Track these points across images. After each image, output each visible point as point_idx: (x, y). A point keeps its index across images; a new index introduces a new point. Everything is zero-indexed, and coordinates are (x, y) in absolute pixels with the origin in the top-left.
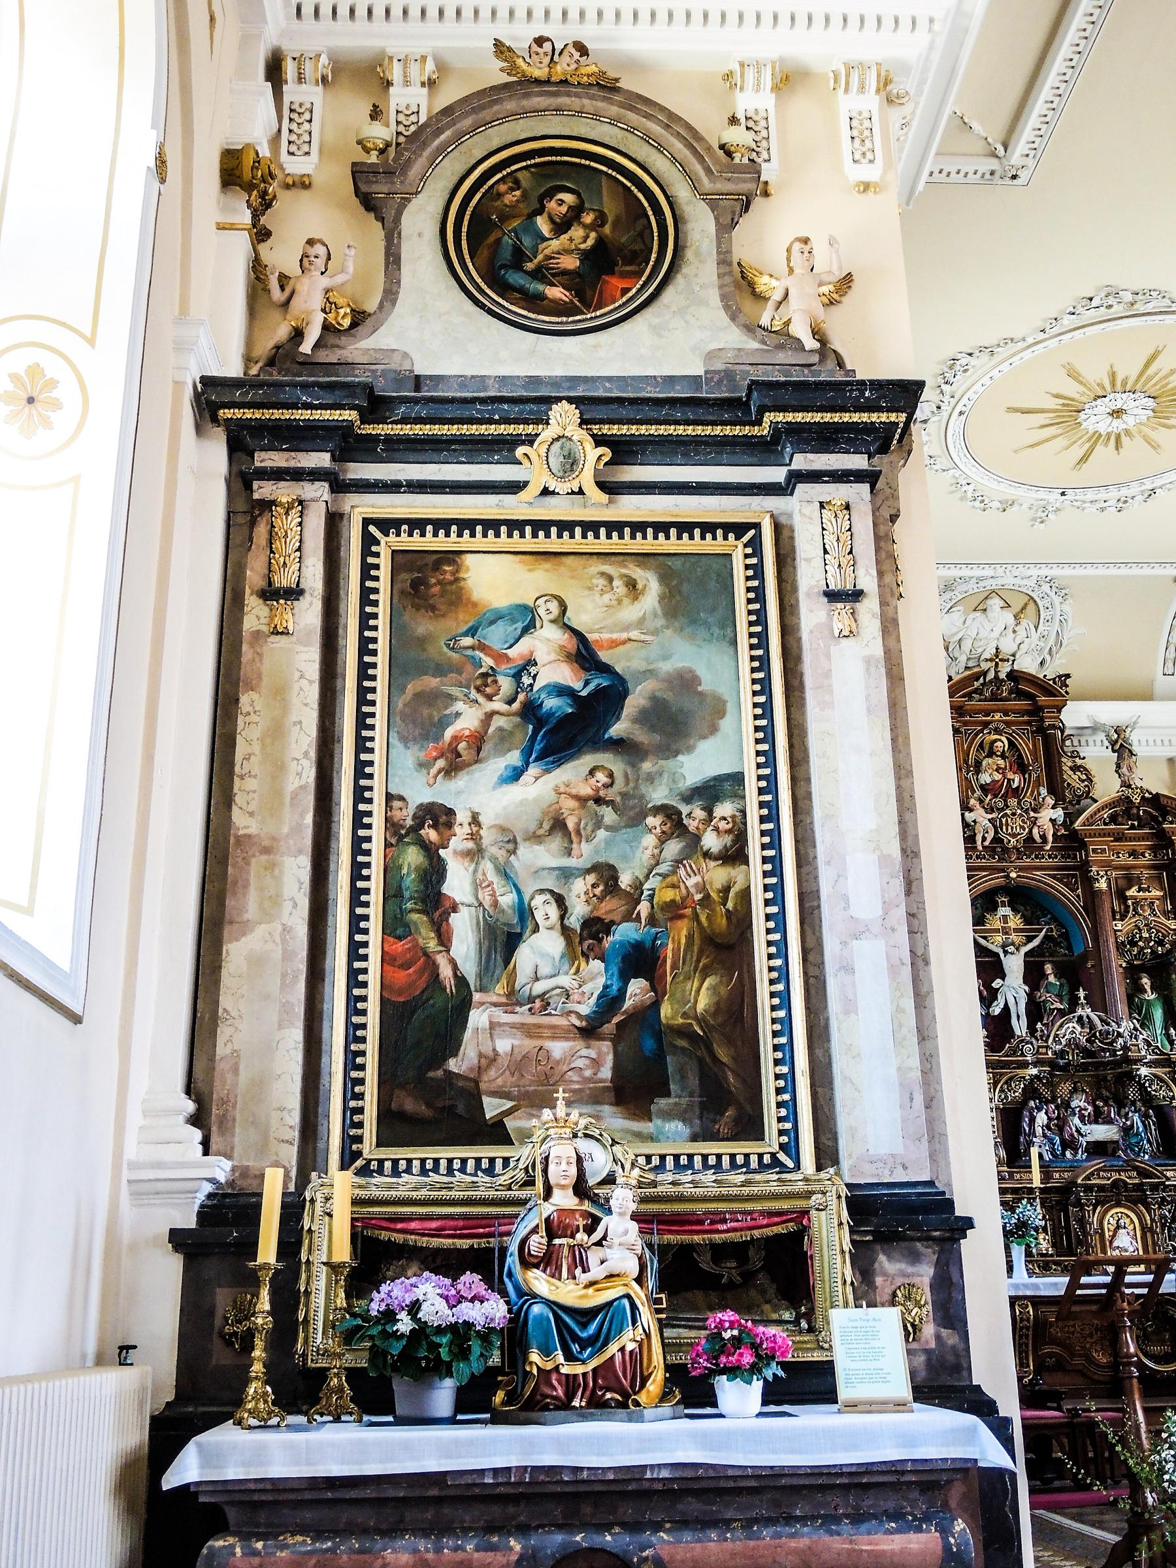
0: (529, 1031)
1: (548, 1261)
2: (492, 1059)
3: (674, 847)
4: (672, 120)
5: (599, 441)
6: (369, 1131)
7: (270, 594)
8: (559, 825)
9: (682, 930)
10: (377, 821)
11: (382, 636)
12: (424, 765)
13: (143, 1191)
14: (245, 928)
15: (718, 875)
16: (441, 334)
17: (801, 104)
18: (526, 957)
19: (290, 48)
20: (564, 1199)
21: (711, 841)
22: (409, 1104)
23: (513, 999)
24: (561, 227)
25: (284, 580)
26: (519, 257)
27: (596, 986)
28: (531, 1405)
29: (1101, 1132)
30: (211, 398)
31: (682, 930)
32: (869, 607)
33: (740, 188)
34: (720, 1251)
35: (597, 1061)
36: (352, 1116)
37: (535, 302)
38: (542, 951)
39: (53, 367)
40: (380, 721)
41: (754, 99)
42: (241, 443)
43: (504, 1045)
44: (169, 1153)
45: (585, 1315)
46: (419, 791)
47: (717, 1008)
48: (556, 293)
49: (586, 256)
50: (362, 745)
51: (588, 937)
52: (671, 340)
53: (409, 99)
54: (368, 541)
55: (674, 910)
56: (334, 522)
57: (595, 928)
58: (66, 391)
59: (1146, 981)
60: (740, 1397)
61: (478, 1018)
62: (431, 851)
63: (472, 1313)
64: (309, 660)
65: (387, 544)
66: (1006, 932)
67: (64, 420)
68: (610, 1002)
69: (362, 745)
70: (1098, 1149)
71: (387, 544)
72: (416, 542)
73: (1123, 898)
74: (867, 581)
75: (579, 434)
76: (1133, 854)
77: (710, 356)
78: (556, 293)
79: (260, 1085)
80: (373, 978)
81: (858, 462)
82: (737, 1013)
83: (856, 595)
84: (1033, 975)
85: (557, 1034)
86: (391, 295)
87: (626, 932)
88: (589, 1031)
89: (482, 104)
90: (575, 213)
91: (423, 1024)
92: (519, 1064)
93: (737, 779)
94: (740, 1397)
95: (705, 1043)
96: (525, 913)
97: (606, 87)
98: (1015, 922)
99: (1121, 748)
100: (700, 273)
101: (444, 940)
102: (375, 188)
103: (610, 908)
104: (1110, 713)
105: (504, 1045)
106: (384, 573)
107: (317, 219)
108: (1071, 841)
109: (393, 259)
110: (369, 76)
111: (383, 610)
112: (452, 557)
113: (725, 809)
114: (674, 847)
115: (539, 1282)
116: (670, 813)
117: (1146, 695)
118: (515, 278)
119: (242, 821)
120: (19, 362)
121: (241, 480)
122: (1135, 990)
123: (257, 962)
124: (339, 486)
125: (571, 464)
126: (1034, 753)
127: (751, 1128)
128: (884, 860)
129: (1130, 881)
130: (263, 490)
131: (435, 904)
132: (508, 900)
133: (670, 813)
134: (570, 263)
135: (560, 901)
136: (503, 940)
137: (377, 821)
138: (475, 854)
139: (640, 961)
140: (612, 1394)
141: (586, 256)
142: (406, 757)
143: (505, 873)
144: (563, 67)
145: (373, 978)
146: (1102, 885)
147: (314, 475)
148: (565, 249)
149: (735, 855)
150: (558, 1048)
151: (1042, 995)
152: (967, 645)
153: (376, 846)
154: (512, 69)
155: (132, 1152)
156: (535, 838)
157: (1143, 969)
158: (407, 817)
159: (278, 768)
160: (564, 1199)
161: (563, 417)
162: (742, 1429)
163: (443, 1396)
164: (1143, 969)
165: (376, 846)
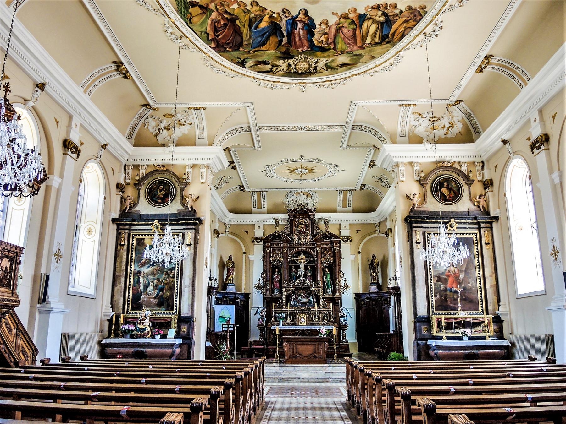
0: (148, 298)
1: (140, 324)
2: (144, 301)
3: (167, 276)
4: (176, 175)
5: (161, 224)
6: (130, 309)
7: (121, 245)
8: (153, 273)
9: (167, 286)
10: (132, 273)
11: (134, 249)
12: (138, 266)
13: (105, 315)
14: (117, 286)
15: (172, 279)
16: (145, 207)
17: (196, 169)
18: (149, 289)
19: (127, 164)
20: (143, 318)
21: (171, 275)
22: (134, 306)
23: (147, 294)
24: (161, 191)
25: (123, 243)
26: (155, 195)
27: (156, 293)
28: (137, 337)
29: (305, 300)
30: (114, 220)
31: (167, 286)
32: (192, 246)
33: (184, 185)
34: (166, 323)
35: (155, 301)
36: (128, 307)
37: (157, 203)
38: (150, 288)
39: (92, 227)
40: (133, 261)
41: (189, 170)
42: (118, 225)
43: (145, 299)
44: (108, 311)
45: (142, 329)
46: (138, 269)
47: (170, 295)
48: (159, 201)
49: (163, 195)
50: (131, 264)
51: (155, 287)
52: (174, 208)
53: (143, 171)
54: (133, 237)
55: (166, 284)
56: (129, 234)
57: (157, 286)
58: (93, 230)
59: (327, 270)
60: (158, 337)
61: (143, 296)
62: (138, 276)
63: (131, 328)
64: (125, 253)
65: (473, 236)
66: (302, 259)
67: (93, 234)
68: (158, 295)
69: (131, 264)
70: (304, 303)
71: (473, 236)
72: (139, 237)
73: (324, 254)
74: (192, 243)
75: (158, 224)
76: (327, 244)
77: (178, 210)
78: (159, 201)
79: (118, 304)
80: (131, 292)
81: (193, 227)
82: (172, 296)
83: (190, 245)
84: (306, 268)
85: (151, 298)
86: (138, 202)
87: (160, 286)
88: (155, 298)
89: (151, 173)
90: (163, 188)
91: (137, 297)
92: (147, 301)
93: (175, 267)
94: (158, 337)
95: (168, 299)
96: (149, 284)
97: (168, 171)
98: (304, 257)
99: (326, 223)
100: (178, 198)
101: (140, 287)
102: (137, 186)
103: (158, 283)
104: (325, 215)
105: (145, 299)
106: (135, 241)
107: (130, 192)
108: (313, 243)
109: (139, 197)
110: (137, 167)
111: (134, 246)
112: (143, 239)
113: (173, 271)
114: (167, 276)
115: (139, 326)
116: (167, 272)
117: (335, 211)
118: (154, 199)
119: (117, 273)
120: (88, 227)
121: (118, 229)
122: (324, 272)
123: (118, 290)
124: (130, 230)
125: (157, 227)
126: (309, 224)
127: (172, 309)
128: (190, 279)
129: (326, 250)
130: (120, 231)
131: (139, 283)
132: (147, 282)
133: (167, 272)
134: (161, 196)
135: (153, 283)
136: (146, 287)
137: (132, 273)
138: (143, 277)
139: (161, 290)
140: (144, 336)
141: (163, 195)
142: (136, 265)
143: (147, 279)
144: (162, 168)
145: (131, 292)
146: (319, 251)
147: (127, 229)
148: (161, 194)
149: (174, 277)
150: (151, 300)
151: (307, 272)
152: (298, 201)
153: (132, 276)
154: (155, 168)
155: (104, 311)
156: (151, 275)
157: (326, 267)
158: (136, 272)
159: (121, 267)
160: (143, 318)
161: (156, 221)
162: (158, 339)
163: (129, 336)
164: (326, 267)
165: (132, 276)
